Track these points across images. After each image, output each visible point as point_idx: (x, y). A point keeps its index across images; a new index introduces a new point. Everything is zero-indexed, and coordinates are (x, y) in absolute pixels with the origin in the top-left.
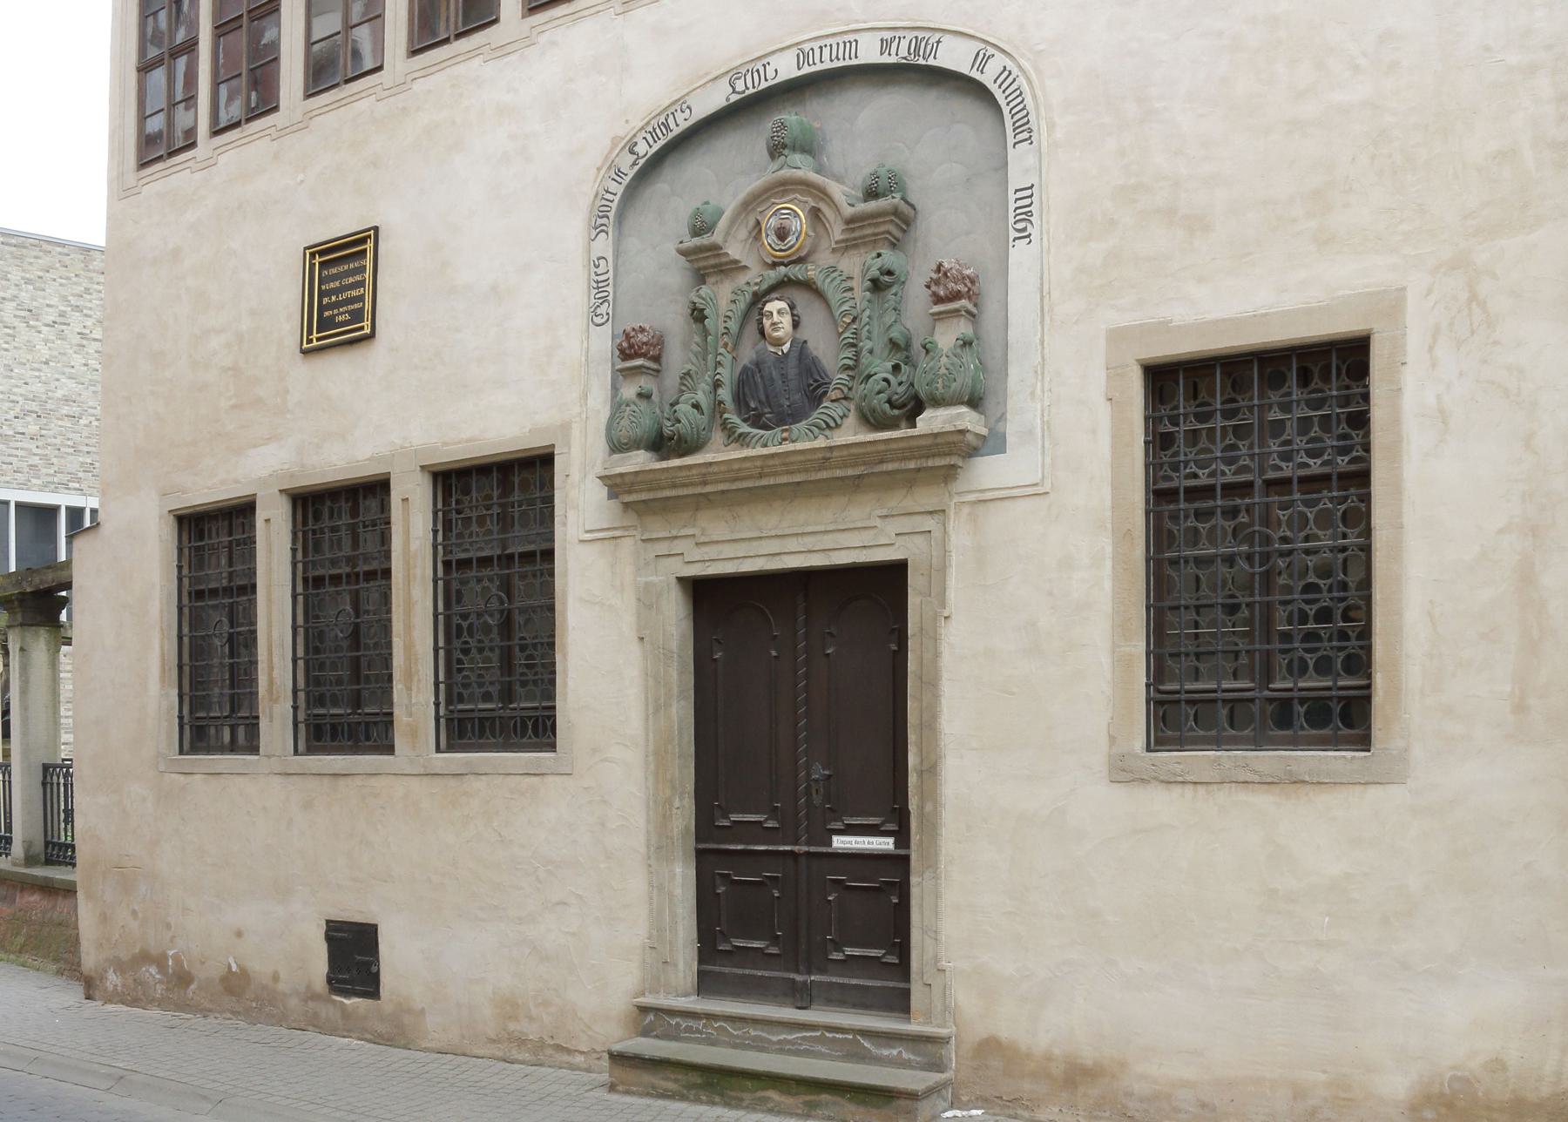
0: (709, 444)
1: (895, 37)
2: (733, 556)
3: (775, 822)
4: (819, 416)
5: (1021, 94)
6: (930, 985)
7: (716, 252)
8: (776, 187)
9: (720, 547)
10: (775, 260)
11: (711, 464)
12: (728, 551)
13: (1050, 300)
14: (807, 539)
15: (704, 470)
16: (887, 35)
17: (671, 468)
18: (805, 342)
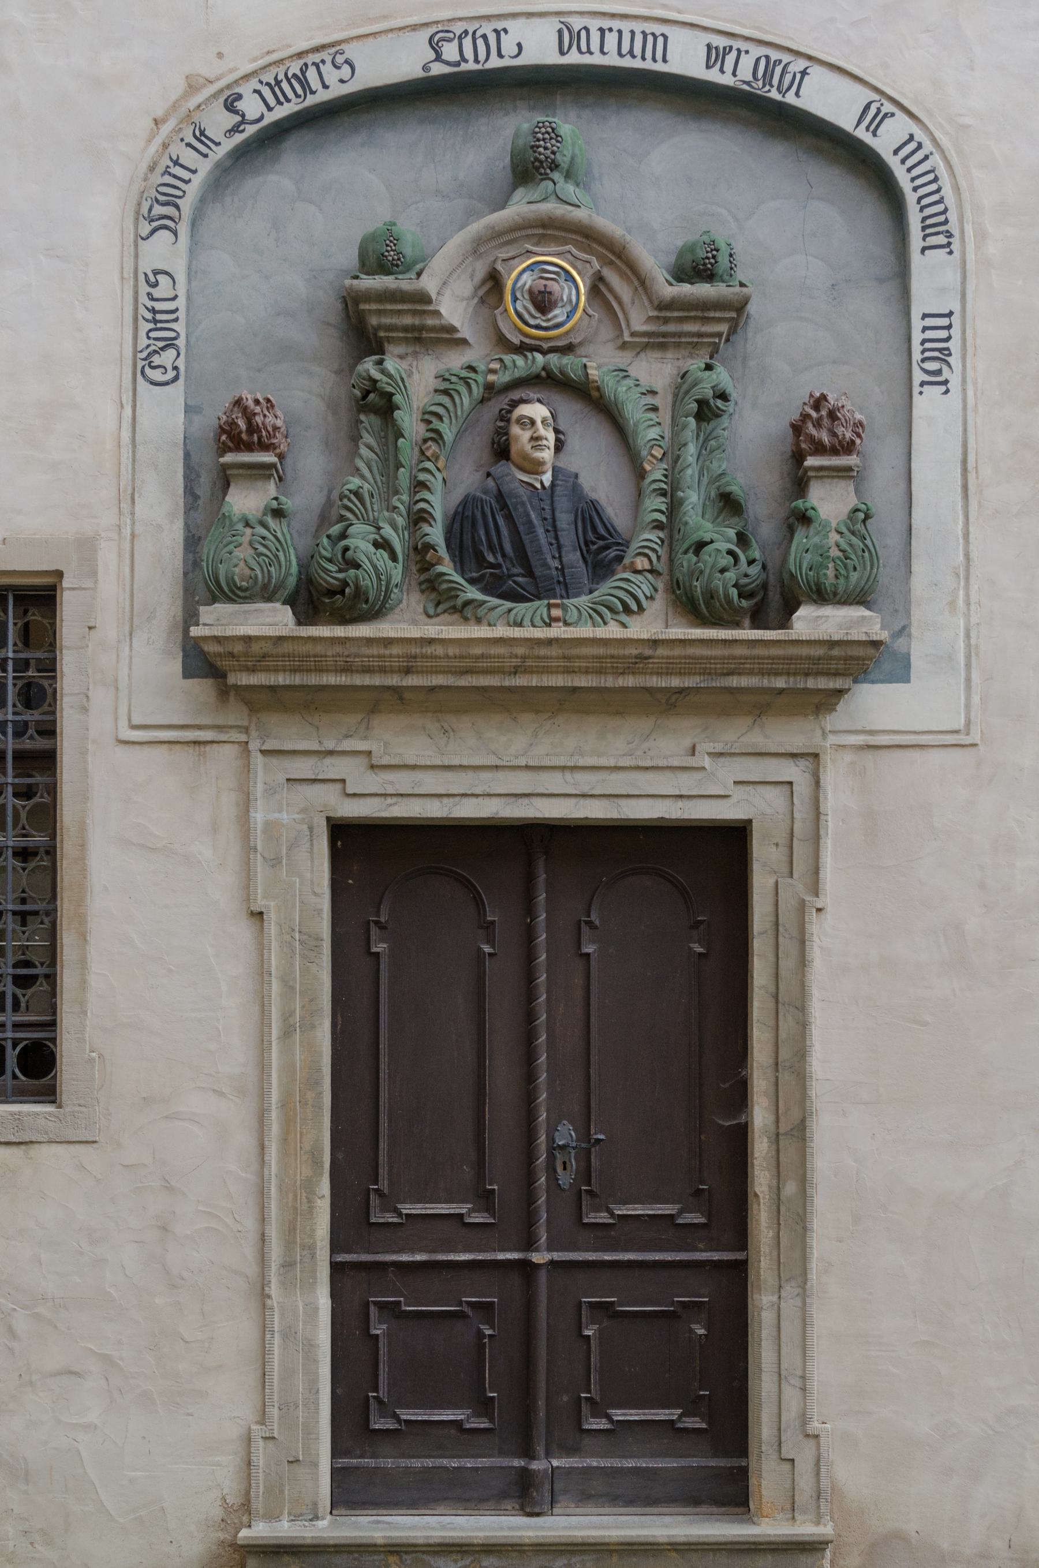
0: (397, 611)
1: (731, 48)
2: (444, 792)
3: (486, 1215)
4: (613, 591)
5: (936, 180)
6: (793, 1460)
7: (418, 307)
8: (531, 227)
9: (419, 775)
10: (527, 341)
11: (431, 641)
12: (431, 782)
13: (977, 478)
14: (580, 777)
15: (415, 650)
16: (720, 42)
17: (353, 639)
18: (576, 476)
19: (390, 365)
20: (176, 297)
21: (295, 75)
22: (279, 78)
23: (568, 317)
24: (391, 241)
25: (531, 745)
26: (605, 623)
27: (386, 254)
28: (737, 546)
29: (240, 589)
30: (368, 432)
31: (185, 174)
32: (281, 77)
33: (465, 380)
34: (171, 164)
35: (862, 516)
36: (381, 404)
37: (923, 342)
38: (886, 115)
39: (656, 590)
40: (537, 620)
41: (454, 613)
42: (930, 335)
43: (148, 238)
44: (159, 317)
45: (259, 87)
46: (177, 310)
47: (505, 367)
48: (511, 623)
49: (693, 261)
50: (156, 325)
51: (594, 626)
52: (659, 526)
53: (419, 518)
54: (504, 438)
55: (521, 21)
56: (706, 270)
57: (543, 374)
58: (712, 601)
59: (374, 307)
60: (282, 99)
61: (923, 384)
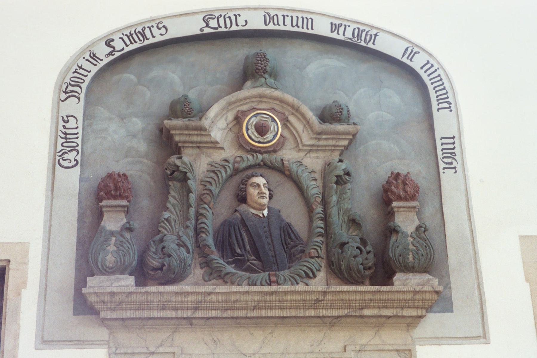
1: (342, 24)
16: (337, 22)
19: (185, 159)
20: (78, 127)
21: (139, 32)
22: (132, 33)
23: (273, 137)
24: (187, 103)
25: (261, 347)
26: (298, 284)
27: (185, 109)
28: (361, 244)
29: (108, 268)
30: (174, 191)
31: (85, 73)
32: (133, 32)
33: (223, 166)
34: (78, 68)
35: (423, 229)
36: (180, 177)
37: (442, 150)
38: (415, 53)
39: (321, 267)
40: (264, 282)
41: (220, 279)
42: (445, 146)
43: (65, 101)
44: (68, 136)
45: (122, 36)
46: (78, 133)
47: (243, 160)
48: (251, 284)
49: (331, 114)
50: (67, 140)
51: (292, 285)
52: (321, 235)
53: (198, 232)
54: (244, 193)
55: (246, 11)
56: (337, 117)
57: (262, 163)
58: (351, 271)
59: (178, 132)
60: (133, 41)
61: (444, 168)
